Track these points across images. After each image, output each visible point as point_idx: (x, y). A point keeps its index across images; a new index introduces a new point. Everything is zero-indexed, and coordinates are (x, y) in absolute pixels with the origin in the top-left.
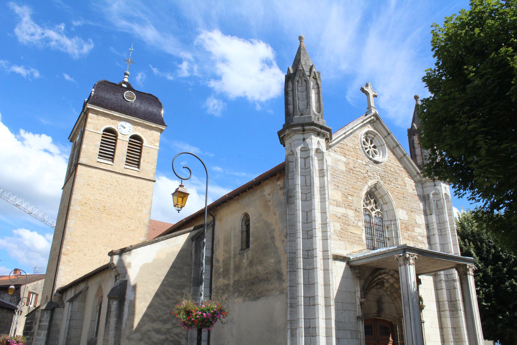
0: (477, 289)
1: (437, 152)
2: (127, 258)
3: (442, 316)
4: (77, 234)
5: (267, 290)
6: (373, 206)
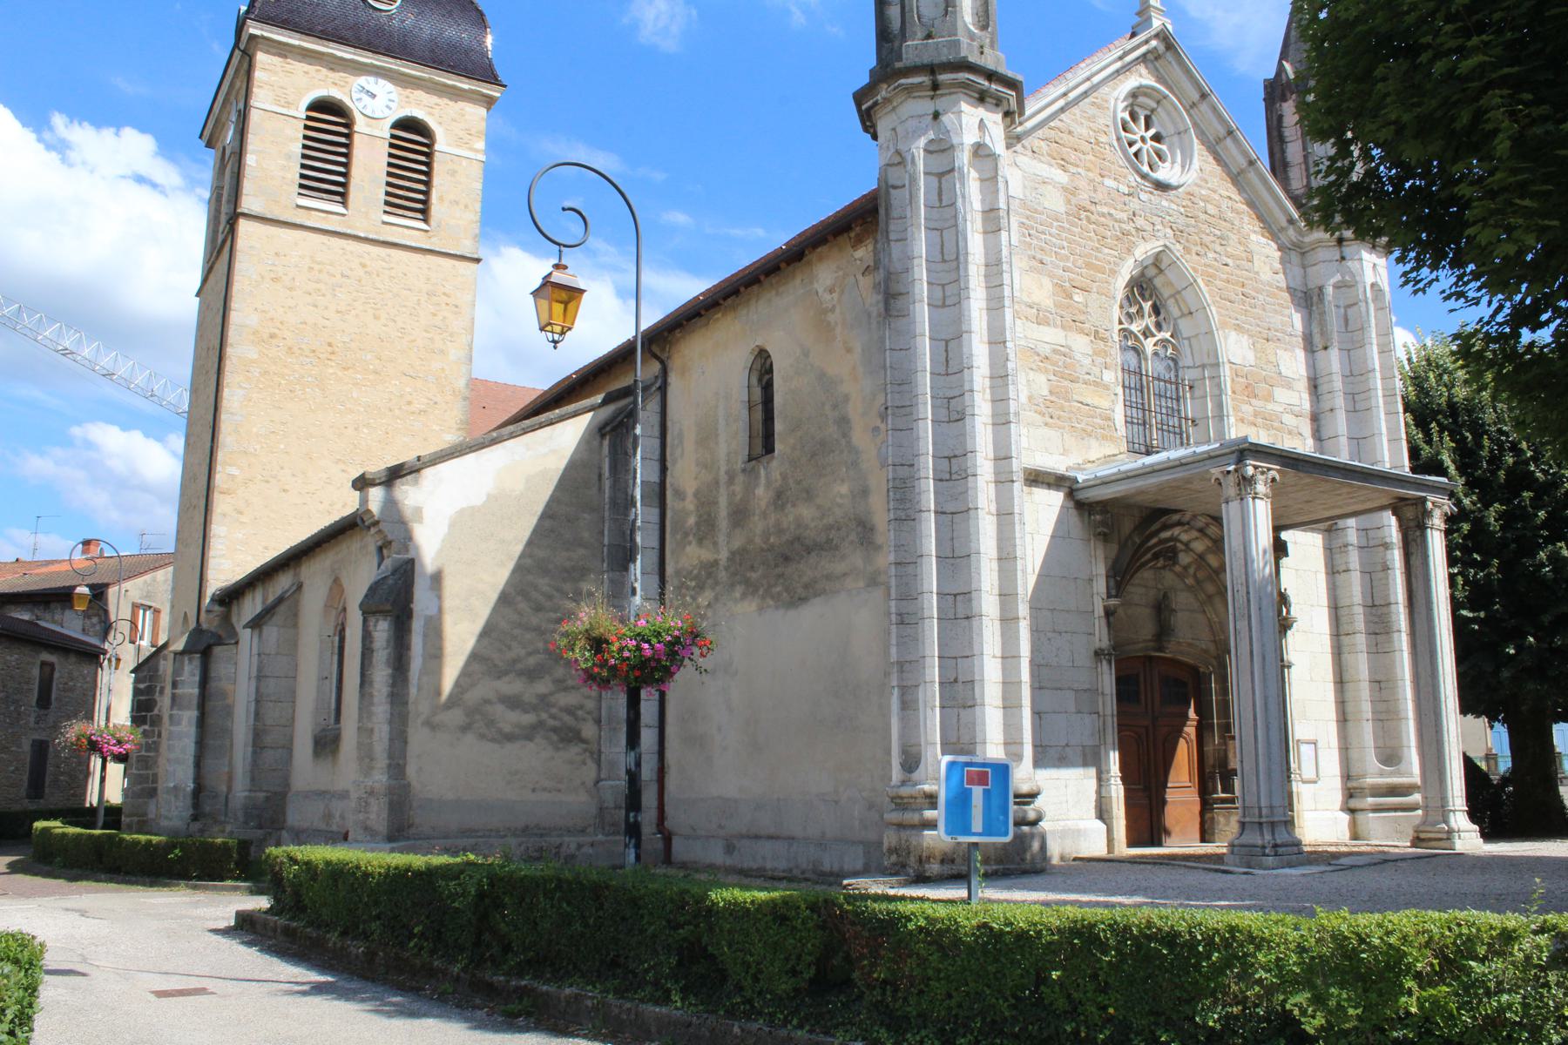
0: (1451, 570)
1: (1352, 148)
2: (409, 494)
3: (1345, 649)
4: (255, 430)
5: (828, 577)
6: (1150, 321)
